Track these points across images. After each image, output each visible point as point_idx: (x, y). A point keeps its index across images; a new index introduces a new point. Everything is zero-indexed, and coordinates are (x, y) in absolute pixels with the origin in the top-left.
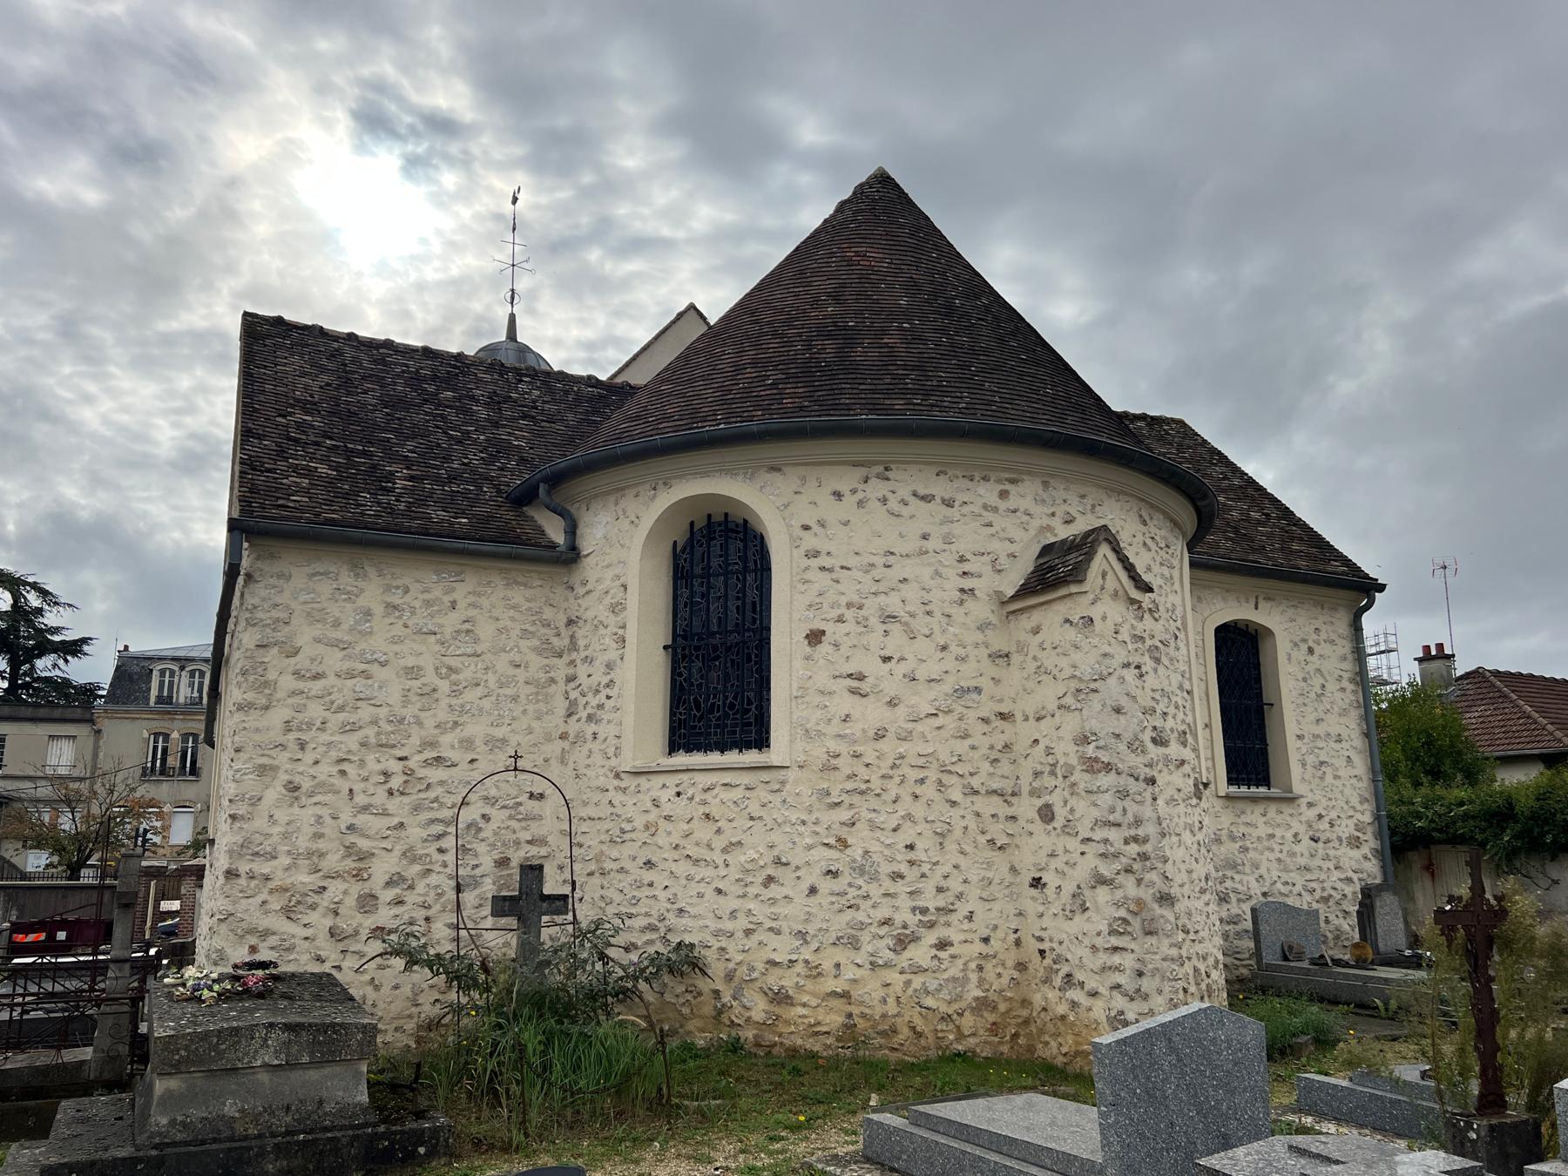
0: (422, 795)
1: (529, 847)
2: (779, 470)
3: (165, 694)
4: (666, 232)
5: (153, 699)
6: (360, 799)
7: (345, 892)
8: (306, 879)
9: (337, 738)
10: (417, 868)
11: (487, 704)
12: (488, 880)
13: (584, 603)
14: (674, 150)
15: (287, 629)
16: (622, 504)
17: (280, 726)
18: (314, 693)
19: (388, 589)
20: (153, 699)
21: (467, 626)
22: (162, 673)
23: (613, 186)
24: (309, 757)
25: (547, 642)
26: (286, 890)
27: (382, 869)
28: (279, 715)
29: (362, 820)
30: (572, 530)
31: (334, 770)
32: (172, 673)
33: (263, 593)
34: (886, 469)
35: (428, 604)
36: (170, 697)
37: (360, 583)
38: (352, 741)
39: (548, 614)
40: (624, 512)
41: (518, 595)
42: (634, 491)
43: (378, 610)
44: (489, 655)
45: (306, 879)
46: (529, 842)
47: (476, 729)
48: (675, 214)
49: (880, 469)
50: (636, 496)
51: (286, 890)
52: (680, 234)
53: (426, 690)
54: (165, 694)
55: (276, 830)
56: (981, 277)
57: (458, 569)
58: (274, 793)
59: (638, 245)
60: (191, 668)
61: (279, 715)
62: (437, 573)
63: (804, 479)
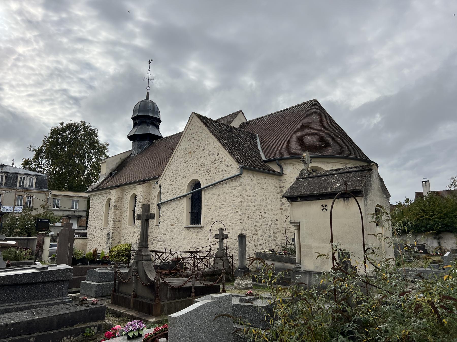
0: (264, 219)
1: (277, 230)
2: (329, 163)
3: (31, 185)
4: (90, 38)
5: (18, 186)
6: (256, 220)
7: (256, 238)
8: (251, 235)
9: (253, 208)
10: (264, 233)
11: (270, 202)
12: (272, 236)
13: (285, 184)
14: (94, 13)
15: (245, 187)
16: (295, 166)
17: (246, 205)
18: (249, 199)
19: (257, 180)
20: (18, 186)
21: (267, 187)
22: (21, 178)
23: (73, 20)
24: (250, 211)
25: (277, 191)
26: (249, 237)
27: (260, 233)
28: (245, 204)
29: (257, 224)
30: (282, 170)
31: (253, 214)
32: (24, 178)
33: (242, 180)
34: (346, 165)
35: (262, 183)
36: (23, 185)
37: (254, 178)
38: (254, 209)
39: (277, 185)
40: (295, 167)
41: (273, 181)
42: (298, 164)
43: (256, 183)
44: (270, 193)
45: (251, 235)
46: (277, 229)
47: (269, 207)
48: (94, 33)
49: (345, 164)
50: (299, 165)
51: (249, 237)
52: (95, 40)
53: (263, 199)
54: (31, 185)
55: (247, 225)
56: (331, 119)
57: (265, 176)
58: (246, 219)
59: (81, 40)
60: (30, 177)
61: (245, 204)
62: (263, 177)
63: (333, 165)
